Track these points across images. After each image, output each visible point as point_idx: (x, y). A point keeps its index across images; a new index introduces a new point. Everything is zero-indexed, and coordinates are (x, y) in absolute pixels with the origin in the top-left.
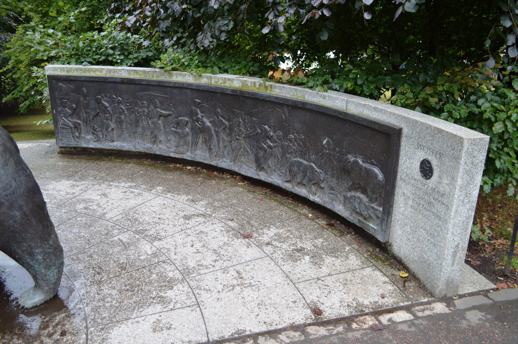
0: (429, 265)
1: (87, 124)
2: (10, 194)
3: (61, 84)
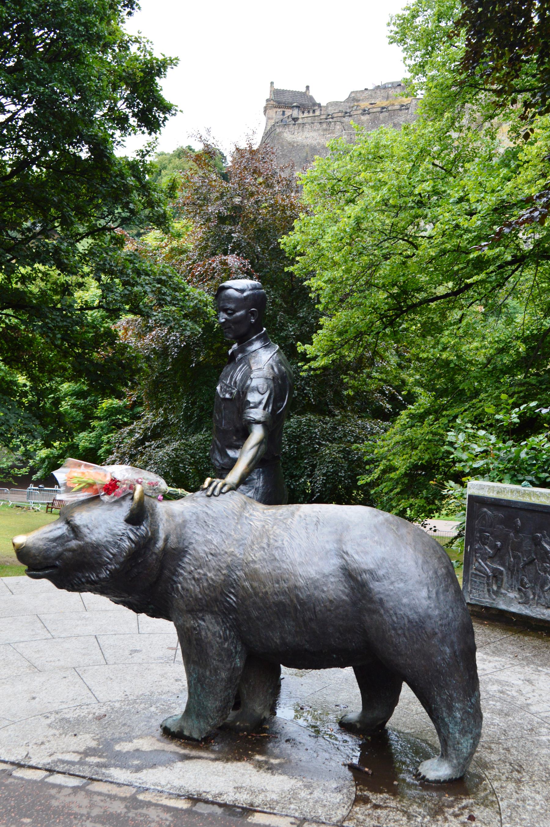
1: (512, 574)
2: (445, 625)
3: (485, 509)
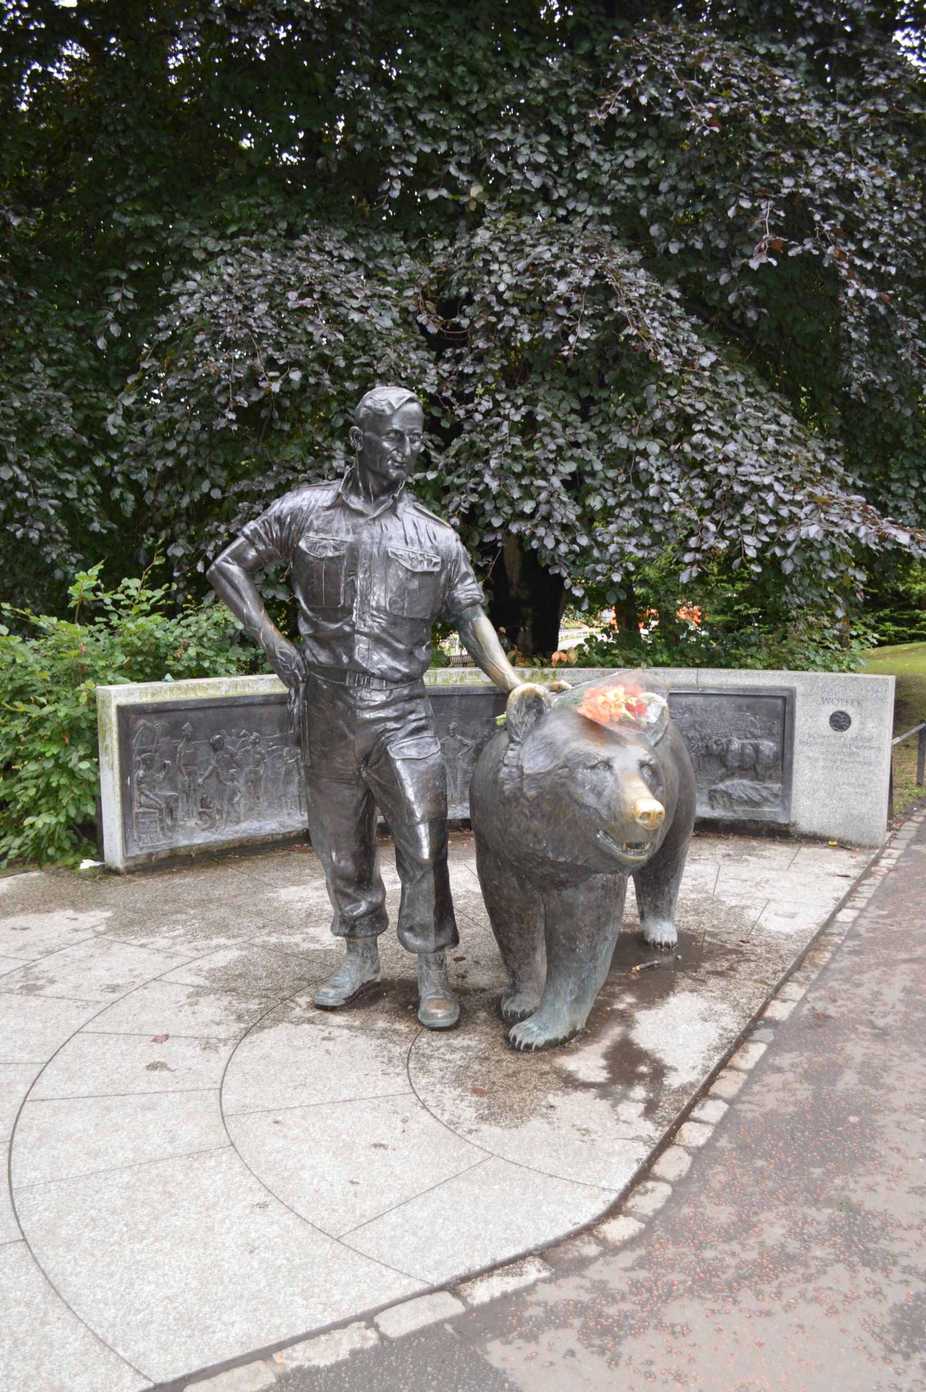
0: (862, 819)
1: (188, 795)
